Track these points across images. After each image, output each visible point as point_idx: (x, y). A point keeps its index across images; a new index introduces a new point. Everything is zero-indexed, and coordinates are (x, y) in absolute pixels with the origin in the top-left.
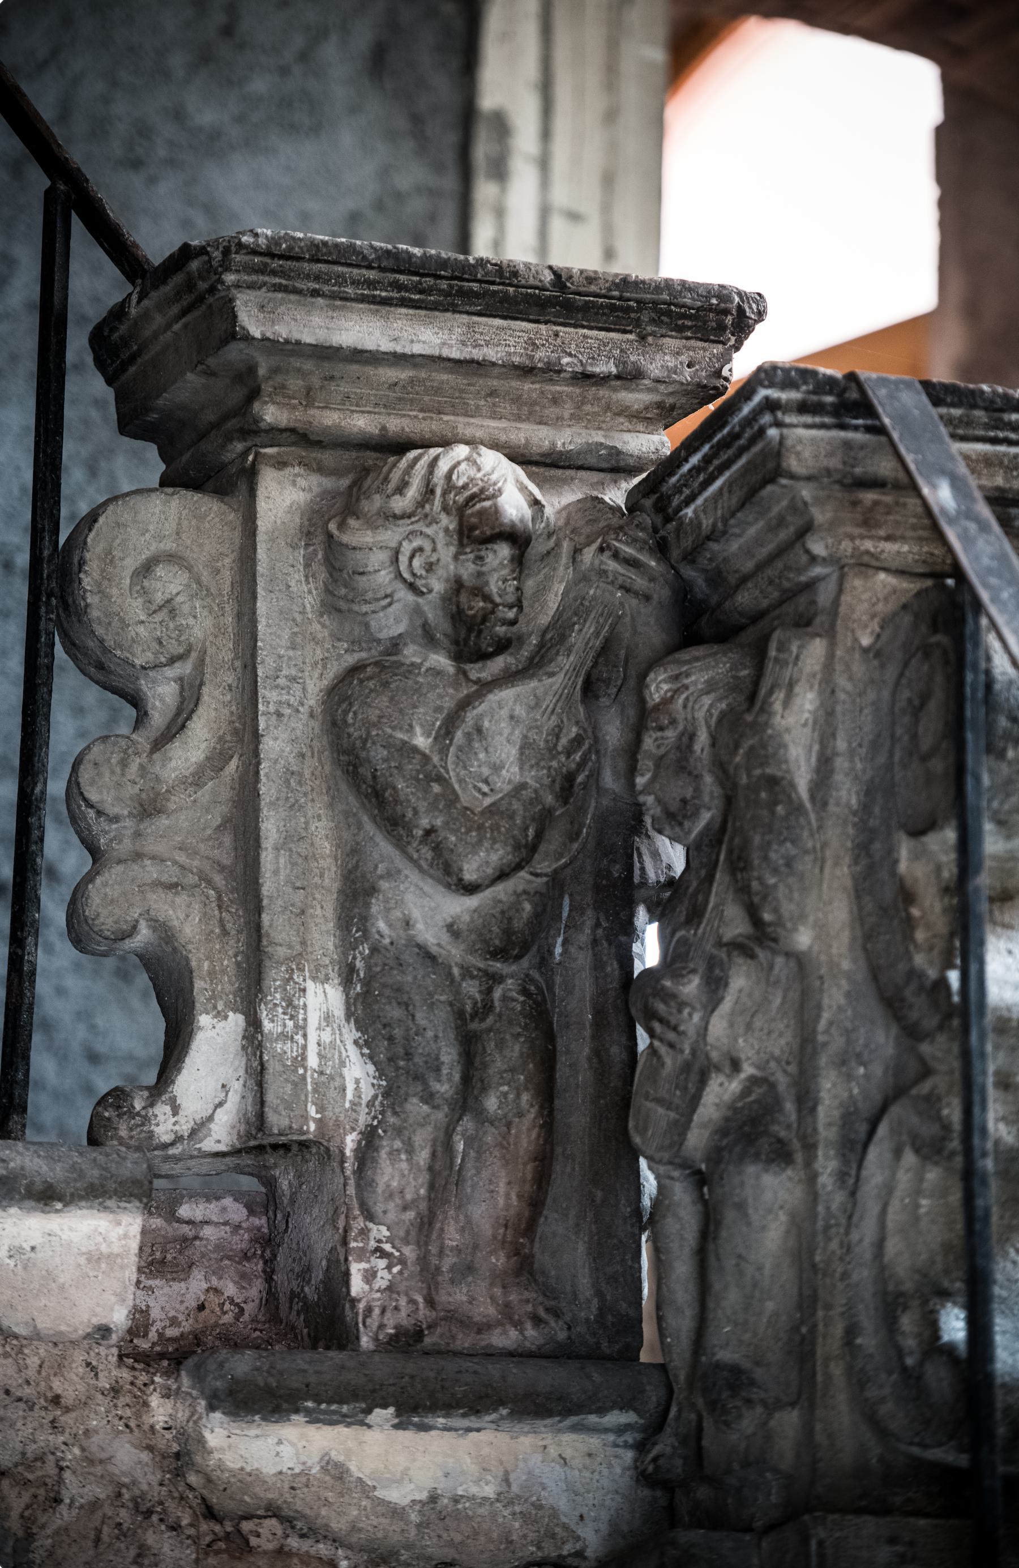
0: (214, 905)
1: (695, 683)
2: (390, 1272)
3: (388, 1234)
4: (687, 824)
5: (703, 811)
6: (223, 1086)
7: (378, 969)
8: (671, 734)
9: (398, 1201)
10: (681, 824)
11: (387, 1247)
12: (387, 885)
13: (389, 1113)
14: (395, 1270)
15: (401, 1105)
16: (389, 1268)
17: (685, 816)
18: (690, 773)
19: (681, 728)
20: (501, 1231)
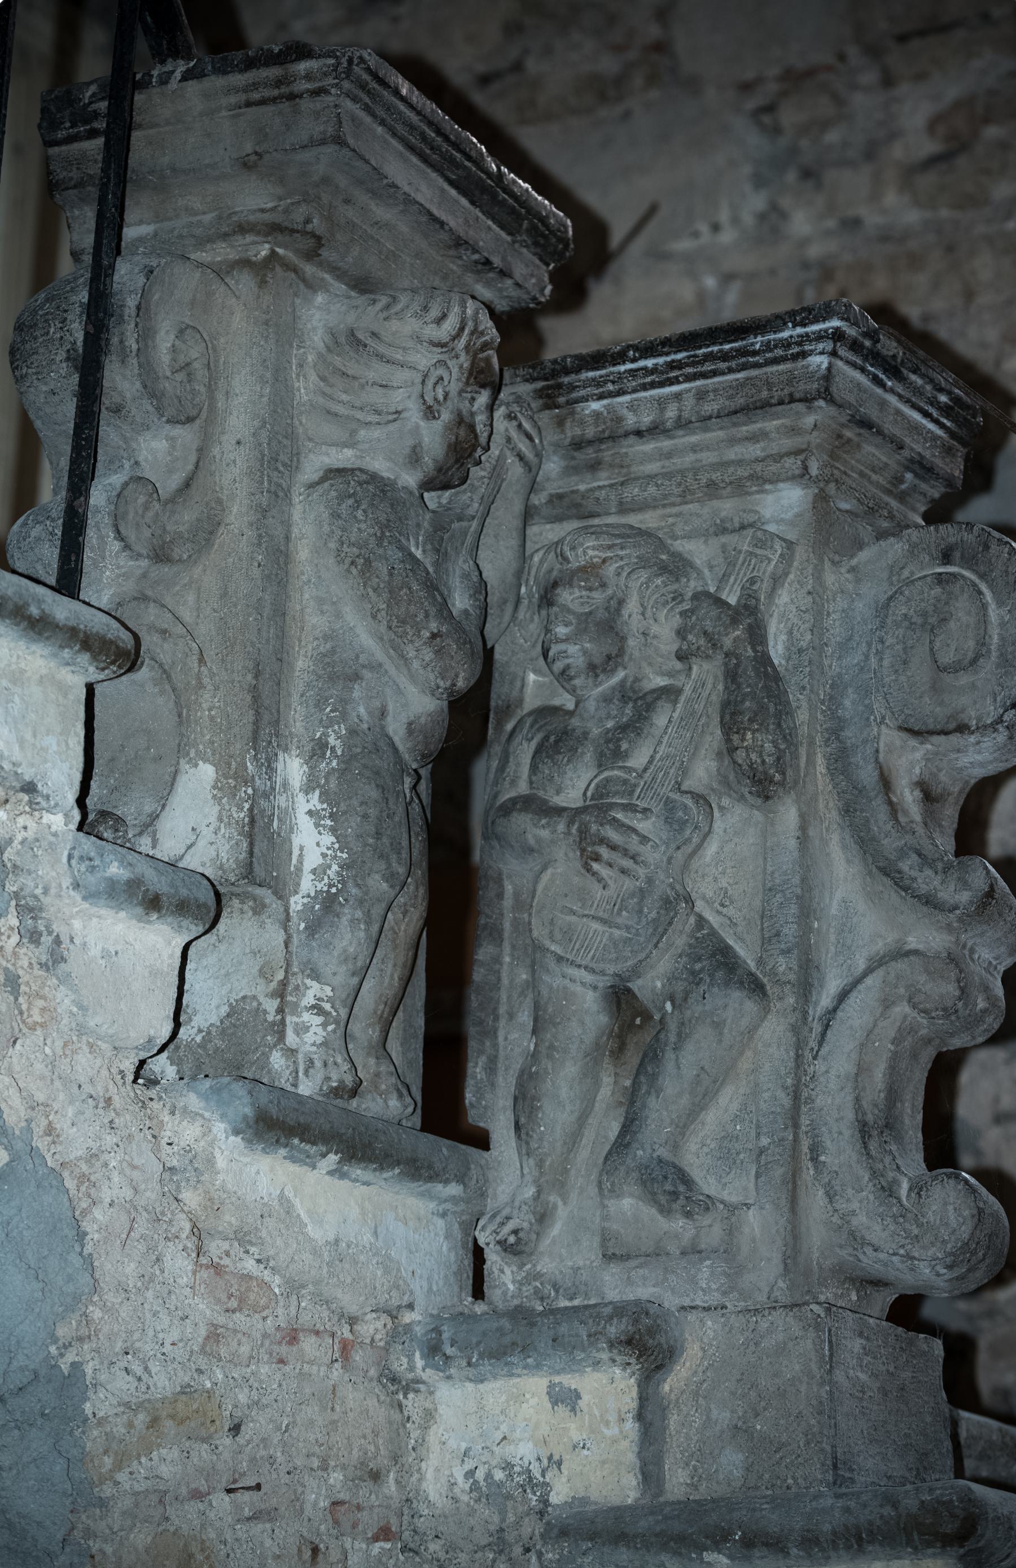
0: (195, 657)
1: (629, 556)
2: (325, 1029)
3: (331, 994)
4: (602, 677)
5: (620, 668)
6: (193, 829)
7: (359, 750)
8: (598, 597)
9: (351, 966)
10: (597, 676)
11: (327, 1007)
12: (370, 675)
13: (350, 884)
14: (330, 1028)
15: (363, 879)
16: (324, 1025)
17: (604, 670)
18: (617, 634)
19: (610, 592)
20: (381, 1007)
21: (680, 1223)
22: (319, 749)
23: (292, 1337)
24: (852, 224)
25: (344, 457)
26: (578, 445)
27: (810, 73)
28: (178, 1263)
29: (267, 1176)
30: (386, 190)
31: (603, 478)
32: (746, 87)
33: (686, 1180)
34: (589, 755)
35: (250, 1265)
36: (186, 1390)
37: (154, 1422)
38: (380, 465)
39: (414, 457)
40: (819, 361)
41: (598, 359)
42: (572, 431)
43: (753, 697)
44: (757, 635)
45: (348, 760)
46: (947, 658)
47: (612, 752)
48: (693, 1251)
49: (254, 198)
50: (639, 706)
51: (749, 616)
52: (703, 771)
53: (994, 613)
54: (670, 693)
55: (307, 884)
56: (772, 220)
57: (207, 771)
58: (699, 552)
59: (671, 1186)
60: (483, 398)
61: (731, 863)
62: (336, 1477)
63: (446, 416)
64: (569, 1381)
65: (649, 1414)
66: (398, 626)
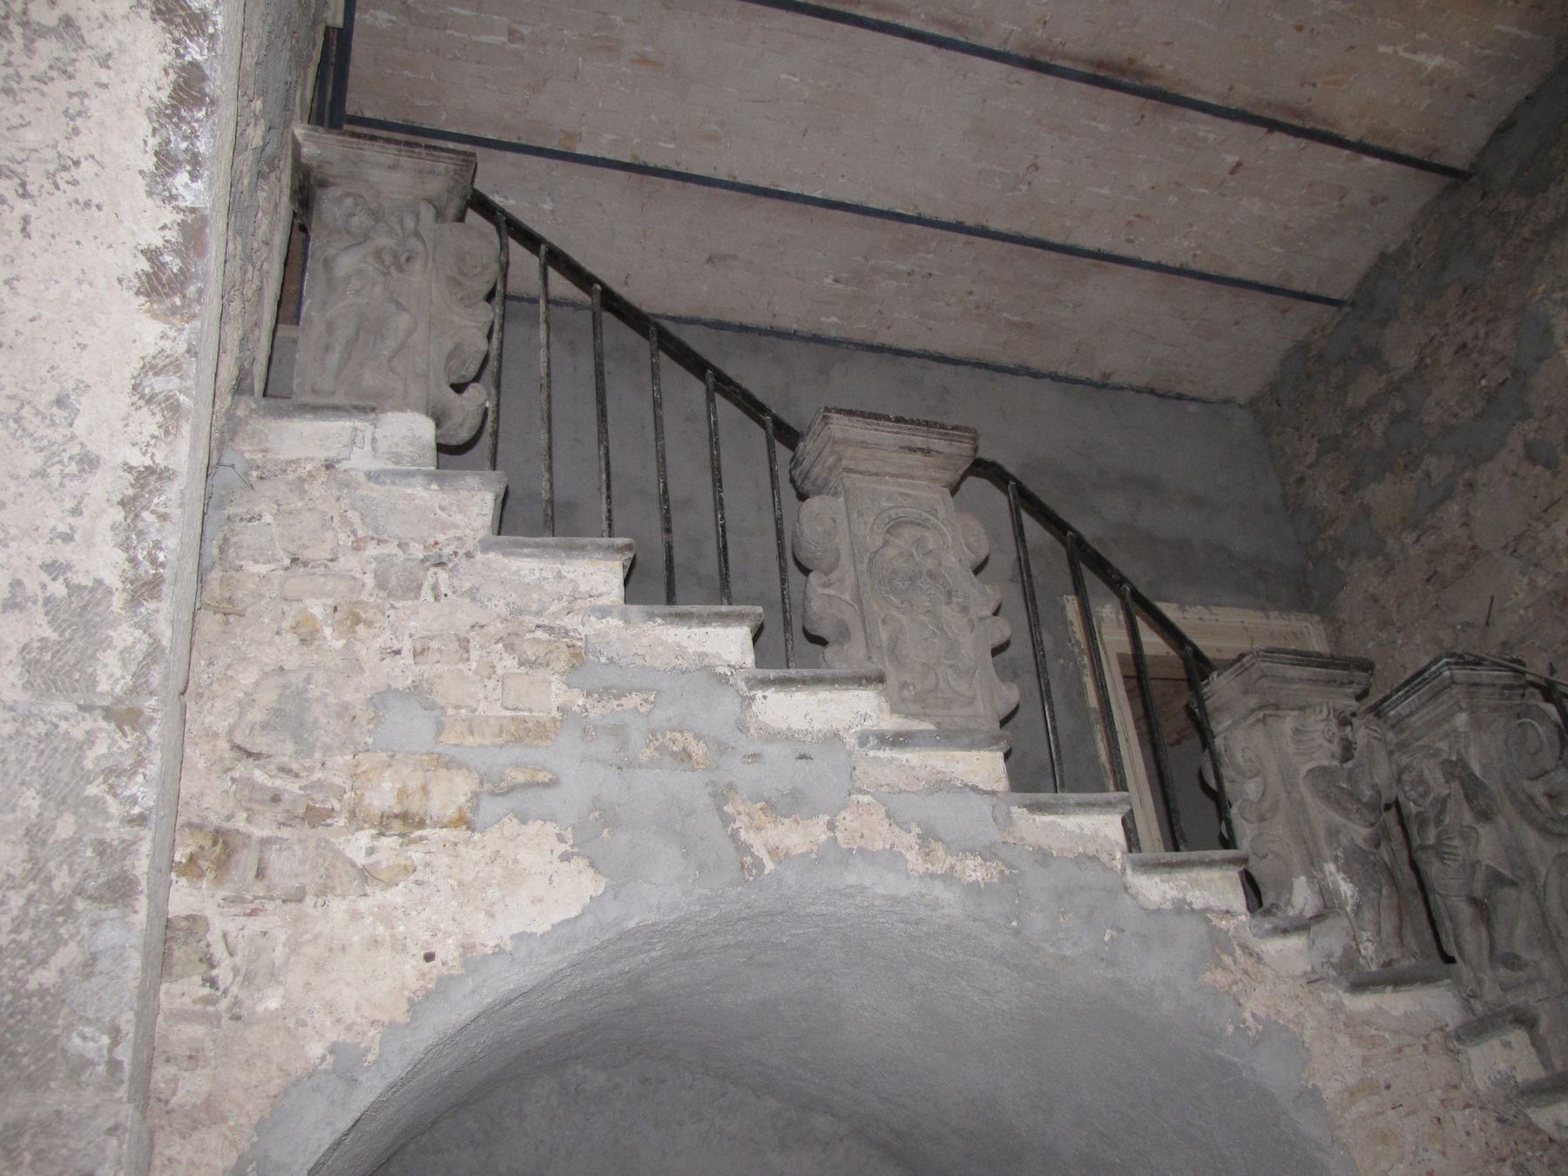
21: (1521, 973)
22: (1336, 859)
23: (1400, 1050)
24: (1557, 575)
25: (1311, 765)
26: (1393, 727)
27: (1523, 534)
28: (1344, 1040)
29: (1363, 1003)
30: (1285, 680)
31: (1406, 734)
32: (1505, 547)
33: (1517, 957)
34: (1432, 823)
35: (1373, 1032)
36: (1362, 1080)
37: (1352, 1094)
38: (1325, 763)
39: (1333, 756)
40: (1447, 673)
41: (1386, 699)
42: (1390, 723)
43: (1472, 788)
44: (1466, 767)
45: (1346, 858)
46: (1532, 750)
47: (1439, 821)
48: (1530, 981)
49: (1253, 701)
50: (1442, 802)
51: (1462, 763)
52: (1468, 818)
53: (1540, 730)
54: (1449, 795)
55: (1350, 901)
56: (1532, 584)
57: (1303, 879)
58: (1443, 745)
59: (1513, 961)
60: (1348, 729)
61: (1488, 847)
62: (1438, 1092)
63: (1336, 740)
64: (1505, 1038)
65: (1537, 1043)
66: (1345, 812)
